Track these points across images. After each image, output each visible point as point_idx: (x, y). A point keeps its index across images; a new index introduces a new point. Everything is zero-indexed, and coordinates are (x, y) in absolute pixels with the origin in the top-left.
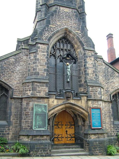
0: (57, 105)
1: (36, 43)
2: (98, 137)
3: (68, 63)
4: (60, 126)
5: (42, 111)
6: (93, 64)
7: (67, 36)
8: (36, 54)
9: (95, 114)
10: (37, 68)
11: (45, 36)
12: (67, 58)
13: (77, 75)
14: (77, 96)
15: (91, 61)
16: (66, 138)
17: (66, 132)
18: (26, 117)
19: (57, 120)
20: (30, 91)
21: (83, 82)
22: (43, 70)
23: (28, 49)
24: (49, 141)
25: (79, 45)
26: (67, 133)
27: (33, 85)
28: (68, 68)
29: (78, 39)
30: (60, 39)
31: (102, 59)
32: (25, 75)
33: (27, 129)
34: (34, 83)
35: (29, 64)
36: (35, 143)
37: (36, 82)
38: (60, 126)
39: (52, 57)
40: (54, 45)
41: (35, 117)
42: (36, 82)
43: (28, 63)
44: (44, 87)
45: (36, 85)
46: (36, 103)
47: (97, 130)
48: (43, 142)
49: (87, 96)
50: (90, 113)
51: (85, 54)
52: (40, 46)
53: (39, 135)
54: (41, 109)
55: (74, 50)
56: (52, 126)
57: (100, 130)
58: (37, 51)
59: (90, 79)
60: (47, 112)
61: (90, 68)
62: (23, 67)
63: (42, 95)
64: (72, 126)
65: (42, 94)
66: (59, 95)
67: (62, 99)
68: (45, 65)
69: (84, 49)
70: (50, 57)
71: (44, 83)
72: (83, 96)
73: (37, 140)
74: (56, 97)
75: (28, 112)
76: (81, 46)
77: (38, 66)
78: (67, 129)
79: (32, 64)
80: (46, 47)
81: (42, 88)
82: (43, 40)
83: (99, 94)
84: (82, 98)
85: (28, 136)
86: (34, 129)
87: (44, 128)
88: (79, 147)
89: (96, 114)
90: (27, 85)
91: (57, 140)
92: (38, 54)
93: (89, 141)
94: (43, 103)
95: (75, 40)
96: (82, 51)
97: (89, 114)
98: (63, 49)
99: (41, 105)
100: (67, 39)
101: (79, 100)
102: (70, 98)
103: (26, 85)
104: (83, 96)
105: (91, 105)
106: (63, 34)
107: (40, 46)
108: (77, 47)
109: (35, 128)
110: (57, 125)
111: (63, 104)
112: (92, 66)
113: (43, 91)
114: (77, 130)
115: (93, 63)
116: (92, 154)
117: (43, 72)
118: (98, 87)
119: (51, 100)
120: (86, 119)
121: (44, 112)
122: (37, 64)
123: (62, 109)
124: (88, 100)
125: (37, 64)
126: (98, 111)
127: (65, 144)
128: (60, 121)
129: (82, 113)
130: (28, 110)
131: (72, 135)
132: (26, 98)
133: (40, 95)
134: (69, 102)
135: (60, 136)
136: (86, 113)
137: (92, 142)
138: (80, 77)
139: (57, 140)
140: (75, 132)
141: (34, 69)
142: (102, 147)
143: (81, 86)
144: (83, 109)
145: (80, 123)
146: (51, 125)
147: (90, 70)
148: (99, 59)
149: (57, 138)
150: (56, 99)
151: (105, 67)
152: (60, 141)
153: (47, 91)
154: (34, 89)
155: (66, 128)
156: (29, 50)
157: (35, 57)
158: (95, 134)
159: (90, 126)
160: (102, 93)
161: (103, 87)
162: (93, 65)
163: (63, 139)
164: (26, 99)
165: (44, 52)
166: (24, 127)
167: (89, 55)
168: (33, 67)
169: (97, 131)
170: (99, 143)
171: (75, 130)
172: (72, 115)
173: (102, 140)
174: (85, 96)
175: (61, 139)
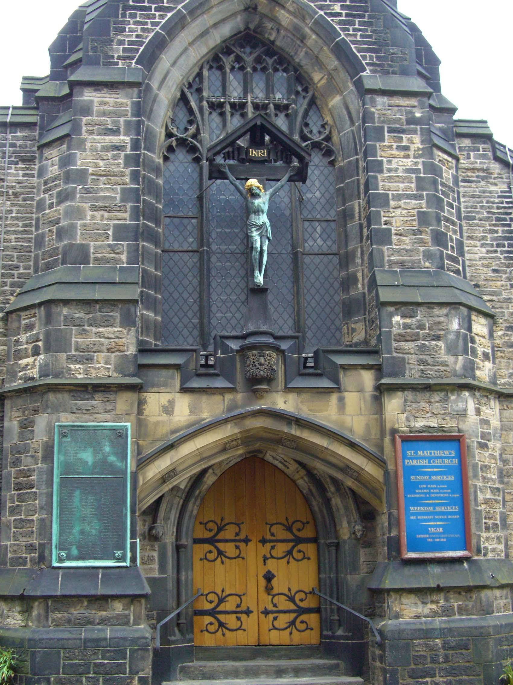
0: (188, 426)
1: (73, 85)
2: (447, 612)
3: (253, 182)
4: (229, 549)
5: (103, 465)
6: (417, 171)
7: (260, 26)
8: (69, 148)
9: (425, 474)
10: (73, 227)
11: (121, 43)
12: (253, 153)
13: (334, 249)
14: (320, 371)
15: (407, 157)
16: (266, 612)
17: (263, 582)
18: (21, 499)
19: (210, 515)
20: (36, 352)
21: (361, 287)
22: (110, 232)
23: (34, 124)
24: (143, 629)
25: (335, 69)
26: (269, 589)
27: (49, 319)
28: (258, 211)
29: (324, 30)
30: (225, 48)
31: (488, 138)
32: (17, 267)
33: (25, 564)
34: (55, 309)
35: (40, 206)
36: (59, 640)
37: (66, 302)
38: (229, 549)
39: (181, 155)
40: (190, 86)
41: (60, 494)
42: (66, 302)
43: (32, 199)
44: (112, 326)
45: (66, 318)
46: (66, 419)
47: (436, 570)
48: (102, 635)
49: (378, 369)
50: (391, 467)
51: (367, 117)
52: (92, 102)
53: (79, 597)
54: (95, 452)
55: (312, 103)
56: (178, 548)
57: (457, 567)
58: (76, 128)
59: (402, 264)
60: (130, 465)
61: (399, 197)
62: (6, 226)
63: (103, 373)
64: (301, 547)
65: (102, 369)
66: (203, 371)
67: (222, 391)
68: (122, 200)
69: (363, 92)
70: (166, 159)
71: (112, 303)
72: (354, 367)
73: (69, 621)
74: (182, 383)
75: (27, 473)
76: (343, 75)
77: (79, 213)
78: (272, 565)
79: (51, 206)
80: (125, 100)
81: (99, 335)
82: (109, 62)
83: (452, 350)
84: (347, 380)
85: (24, 601)
86: (55, 564)
87: (113, 558)
88: (337, 666)
89: (436, 473)
90: (24, 322)
91: (211, 624)
92: (81, 144)
93: (381, 632)
94: (108, 416)
95: (309, 43)
96: (354, 103)
97: (386, 474)
98: (243, 106)
99: (95, 429)
100: (264, 44)
101: (328, 391)
102: (269, 380)
103: (19, 321)
104: (354, 367)
105: (403, 417)
106: (234, 15)
107: (92, 102)
108: (324, 81)
109: (60, 560)
110: (211, 541)
111: (226, 421)
112: (413, 185)
113: (104, 348)
114: (330, 568)
115: (420, 167)
117: (110, 246)
118: (445, 311)
119: (155, 400)
120: (374, 502)
121: (111, 465)
122: (76, 203)
123: (224, 450)
124: (382, 391)
125: (76, 203)
126: (446, 456)
127: (261, 650)
128: (226, 521)
129: (347, 468)
130: (26, 461)
131: (302, 595)
133: (86, 371)
134: (263, 404)
135: (230, 605)
136: (370, 469)
137: (403, 640)
138: (346, 259)
139: (211, 624)
140: (320, 580)
141: (61, 234)
142: (466, 671)
143: (350, 309)
144: (352, 445)
145: (347, 528)
146: (169, 539)
147: (398, 211)
148: (467, 142)
149: (212, 613)
150: (184, 390)
151: (505, 188)
152: (227, 633)
153: (132, 350)
154: (54, 343)
155: (265, 559)
156: (42, 128)
157: (66, 161)
158: (421, 592)
159: (395, 545)
160: (483, 346)
161: (492, 311)
162: (418, 179)
163: (250, 622)
164: (19, 401)
165: (115, 132)
166: (10, 555)
167: (389, 121)
168: (58, 221)
169: (434, 576)
170: (446, 646)
171: (319, 572)
172: (300, 482)
173: (462, 625)
175: (238, 619)
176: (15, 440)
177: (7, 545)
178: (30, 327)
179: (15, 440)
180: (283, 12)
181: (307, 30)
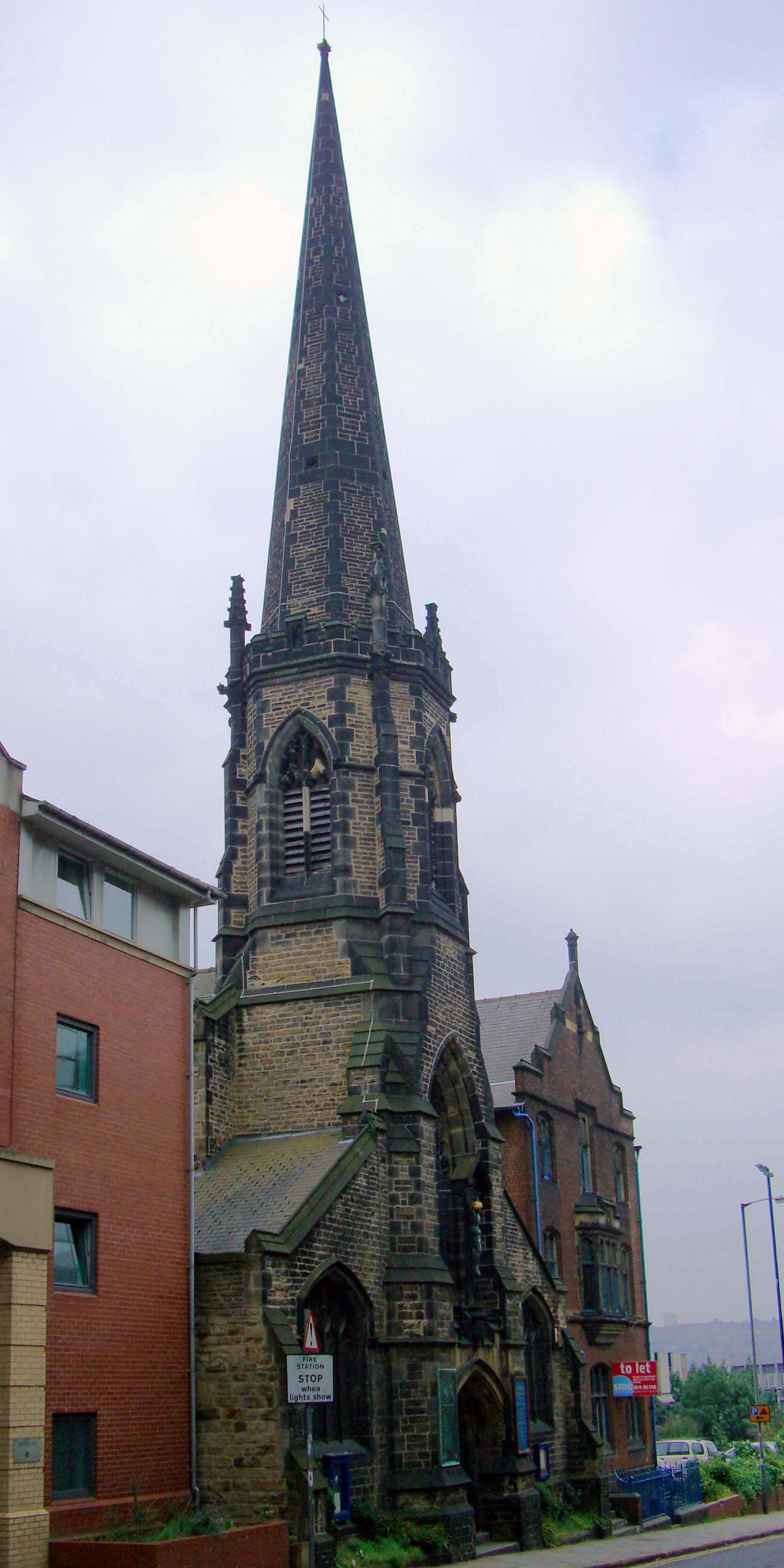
75: (418, 1403)
79: (404, 1203)
116: (523, 1547)
130: (416, 1395)
132: (406, 1345)
174: (85, 1031)
176: (405, 1378)
177: (401, 1455)
178: (413, 1297)
179: (405, 1378)
180: (454, 1063)
181: (461, 1079)
